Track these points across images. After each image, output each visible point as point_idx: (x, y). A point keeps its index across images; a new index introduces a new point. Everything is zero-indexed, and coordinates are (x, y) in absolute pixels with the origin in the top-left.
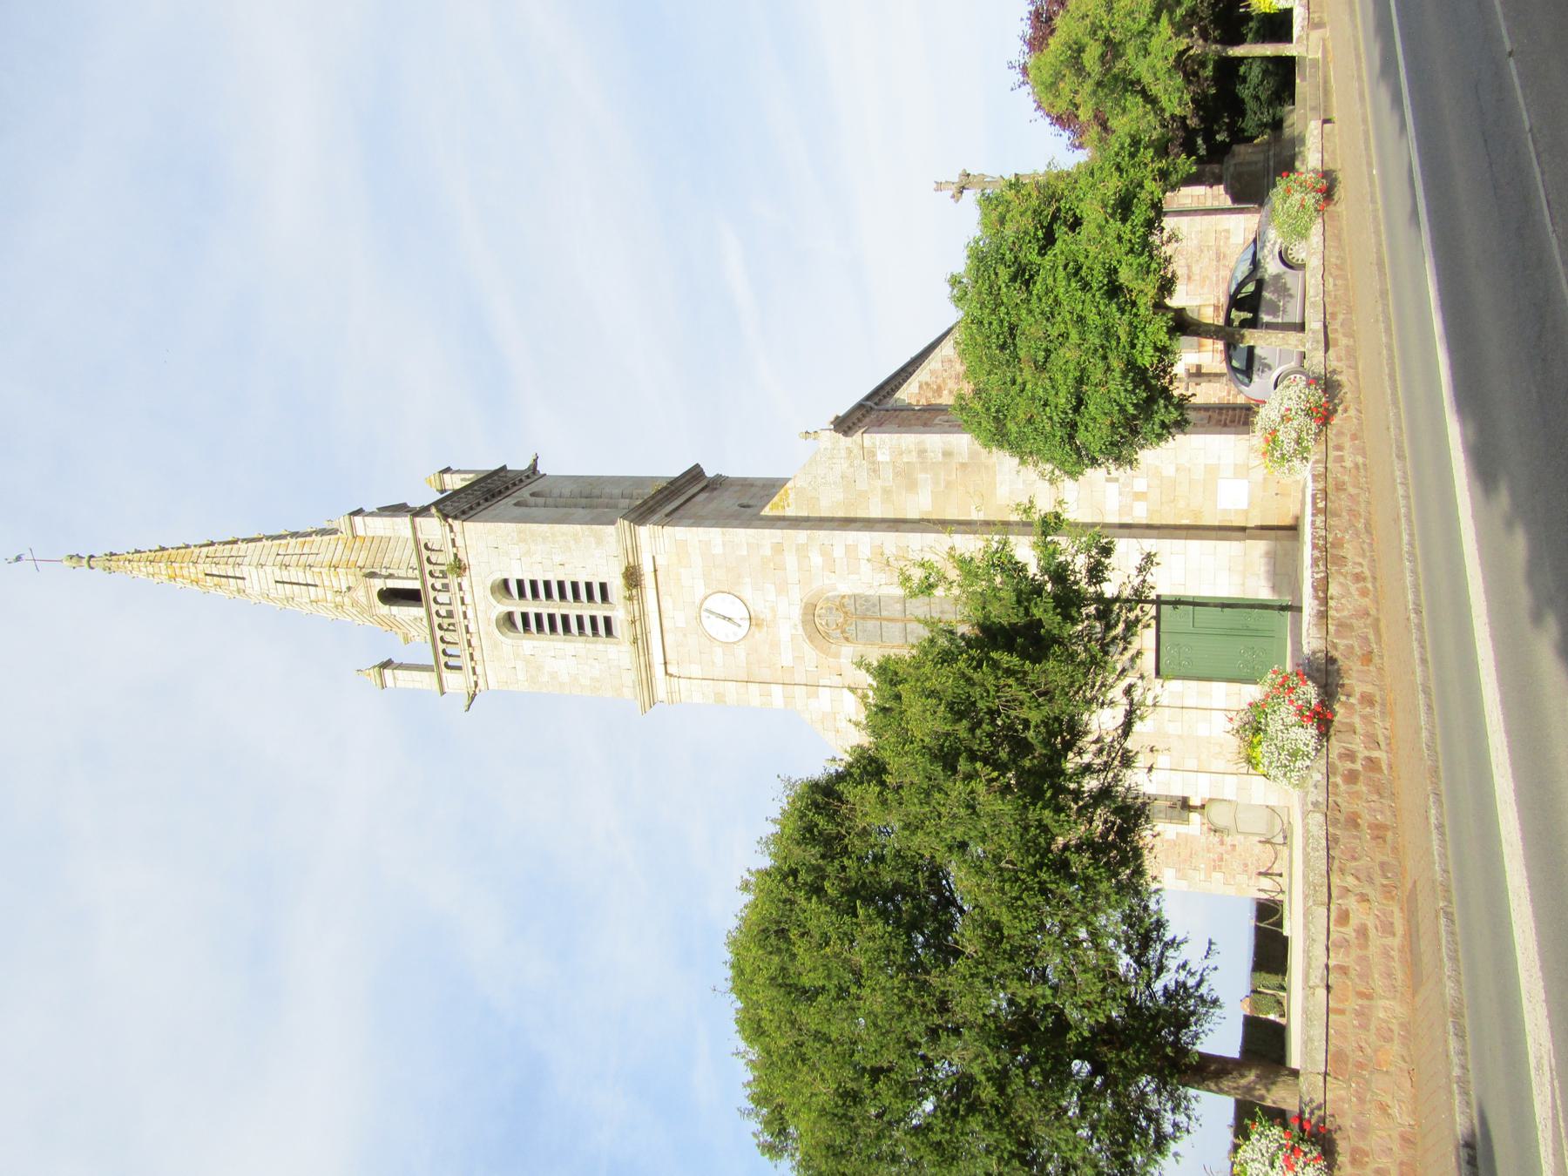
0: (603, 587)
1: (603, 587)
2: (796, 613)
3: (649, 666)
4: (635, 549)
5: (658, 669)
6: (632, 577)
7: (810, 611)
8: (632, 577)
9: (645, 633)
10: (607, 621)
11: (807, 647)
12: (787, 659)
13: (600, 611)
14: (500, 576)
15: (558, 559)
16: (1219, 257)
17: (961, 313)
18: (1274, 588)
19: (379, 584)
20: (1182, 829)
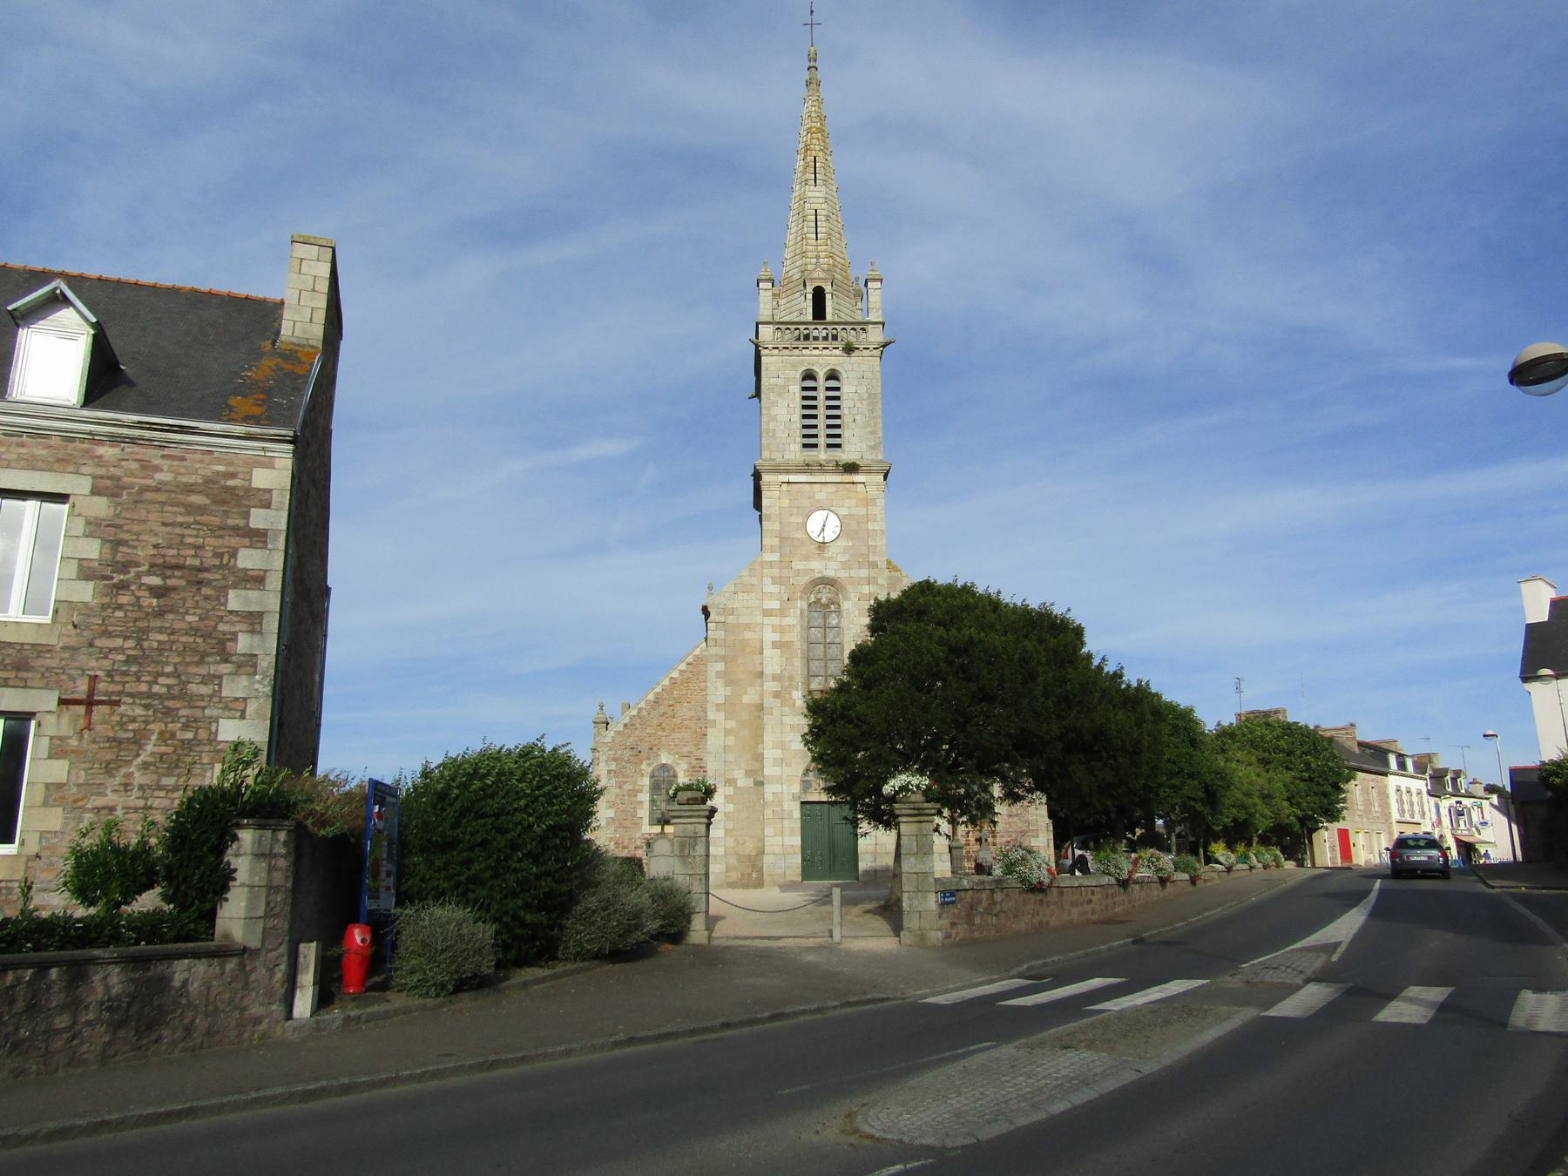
0: (839, 446)
1: (839, 446)
2: (830, 573)
3: (788, 472)
4: (869, 472)
5: (785, 478)
6: (851, 468)
7: (830, 582)
8: (851, 468)
9: (811, 472)
10: (815, 446)
11: (807, 579)
12: (797, 565)
13: (822, 441)
14: (843, 376)
15: (858, 418)
16: (1023, 833)
17: (111, 512)
18: (866, 872)
19: (828, 288)
20: (646, 820)
